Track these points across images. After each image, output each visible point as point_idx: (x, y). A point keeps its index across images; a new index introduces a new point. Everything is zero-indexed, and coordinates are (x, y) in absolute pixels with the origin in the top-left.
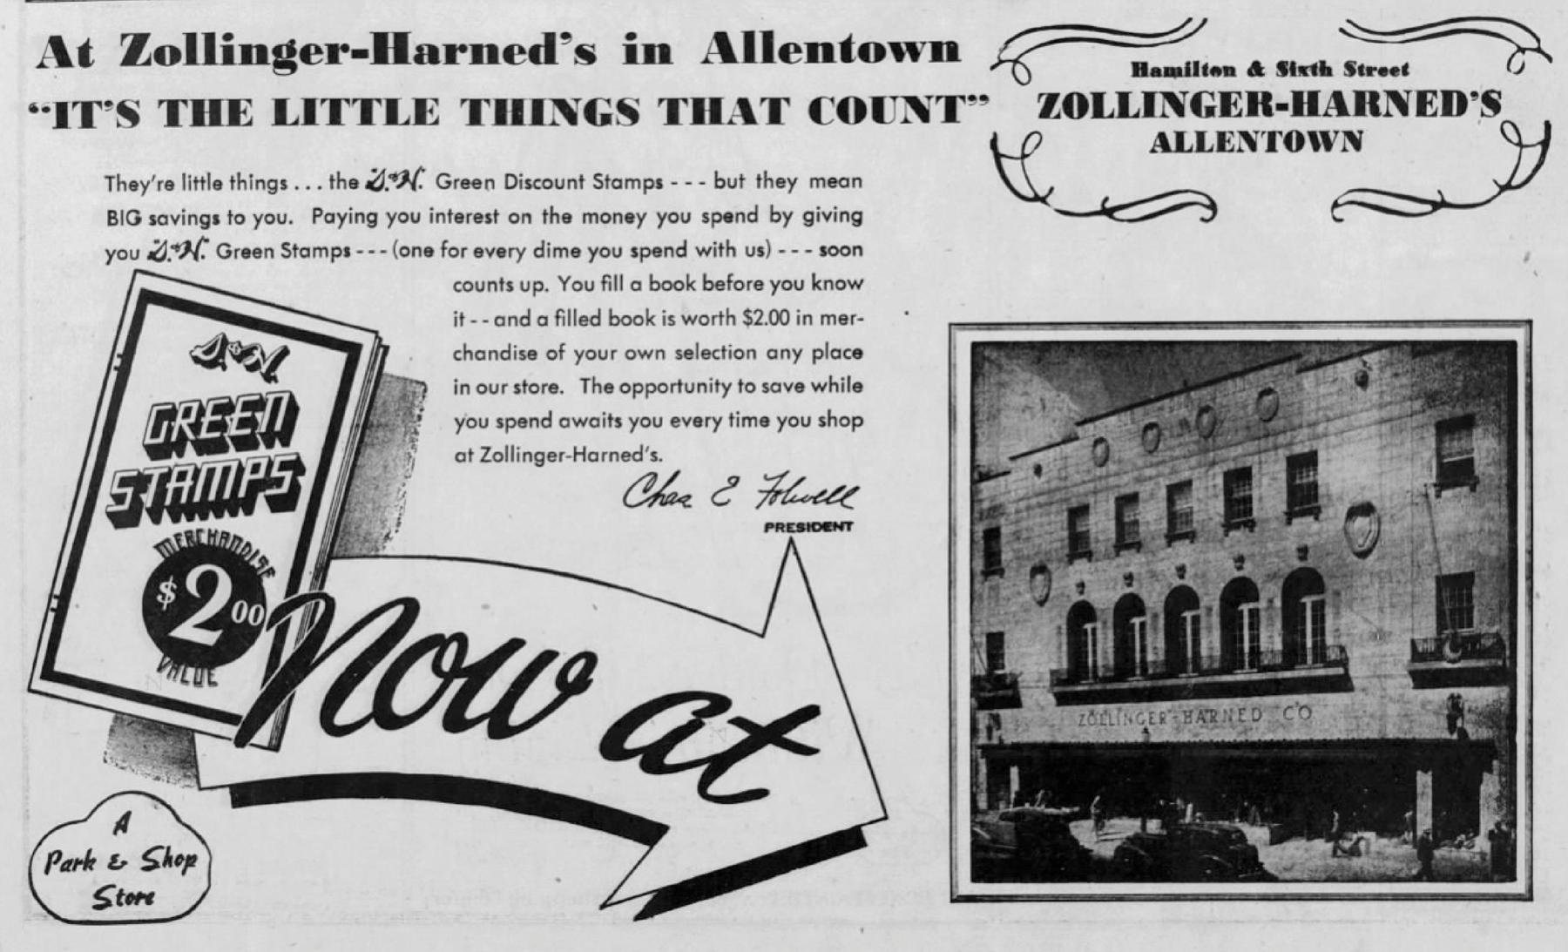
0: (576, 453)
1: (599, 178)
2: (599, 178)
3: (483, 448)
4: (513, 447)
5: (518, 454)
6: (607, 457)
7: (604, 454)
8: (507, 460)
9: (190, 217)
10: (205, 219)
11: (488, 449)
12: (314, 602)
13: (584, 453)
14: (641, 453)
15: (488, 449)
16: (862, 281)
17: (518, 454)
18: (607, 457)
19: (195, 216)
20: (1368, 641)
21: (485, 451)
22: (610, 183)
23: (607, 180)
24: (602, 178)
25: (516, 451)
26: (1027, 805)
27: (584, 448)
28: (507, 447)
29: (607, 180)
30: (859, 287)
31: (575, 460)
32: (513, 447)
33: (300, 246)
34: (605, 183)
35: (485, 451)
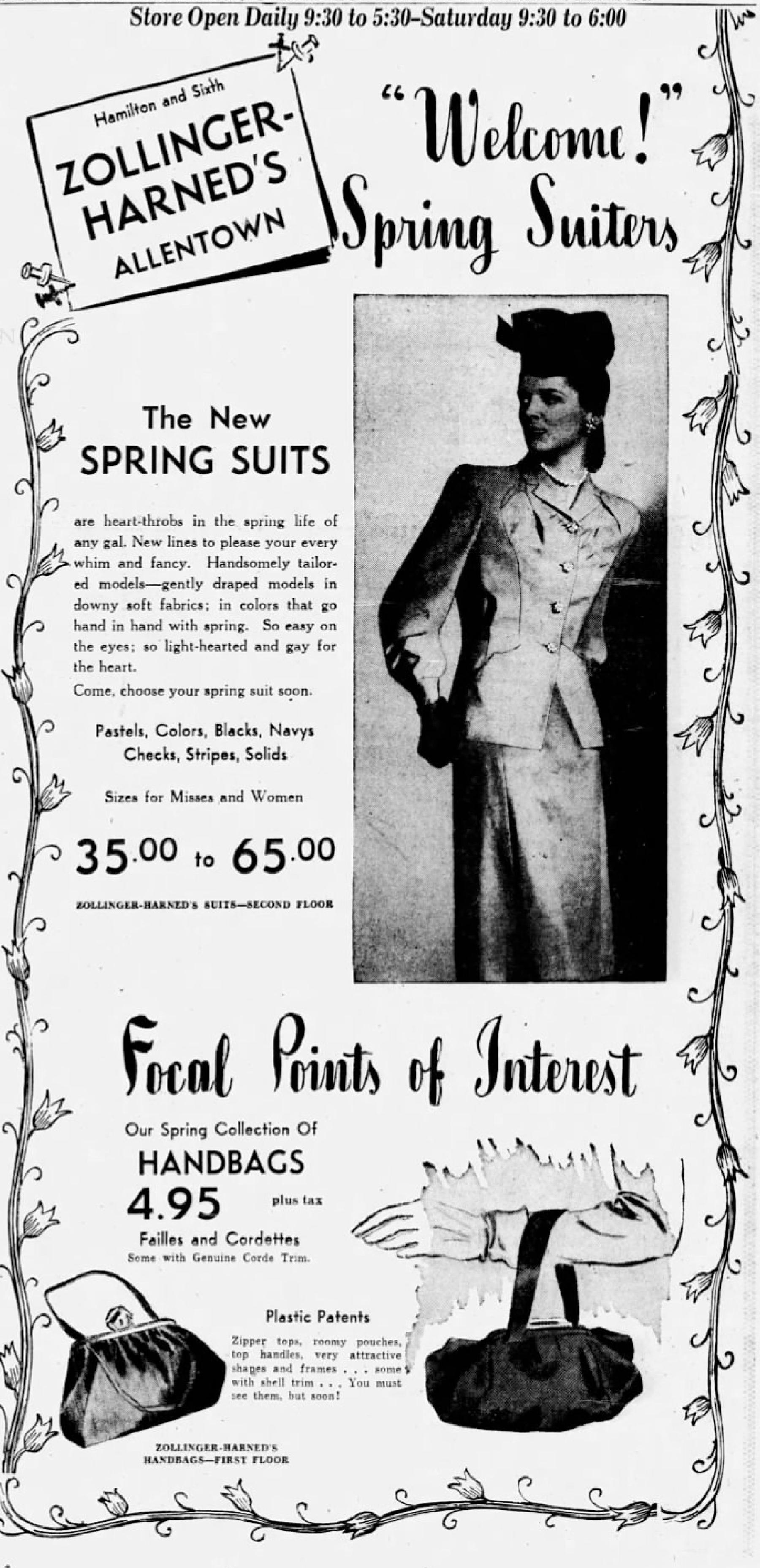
3: (59, 167)
16: (268, 416)
21: (65, 171)
22: (201, 861)
23: (198, 754)
27: (217, 557)
30: (264, 424)
35: (65, 171)
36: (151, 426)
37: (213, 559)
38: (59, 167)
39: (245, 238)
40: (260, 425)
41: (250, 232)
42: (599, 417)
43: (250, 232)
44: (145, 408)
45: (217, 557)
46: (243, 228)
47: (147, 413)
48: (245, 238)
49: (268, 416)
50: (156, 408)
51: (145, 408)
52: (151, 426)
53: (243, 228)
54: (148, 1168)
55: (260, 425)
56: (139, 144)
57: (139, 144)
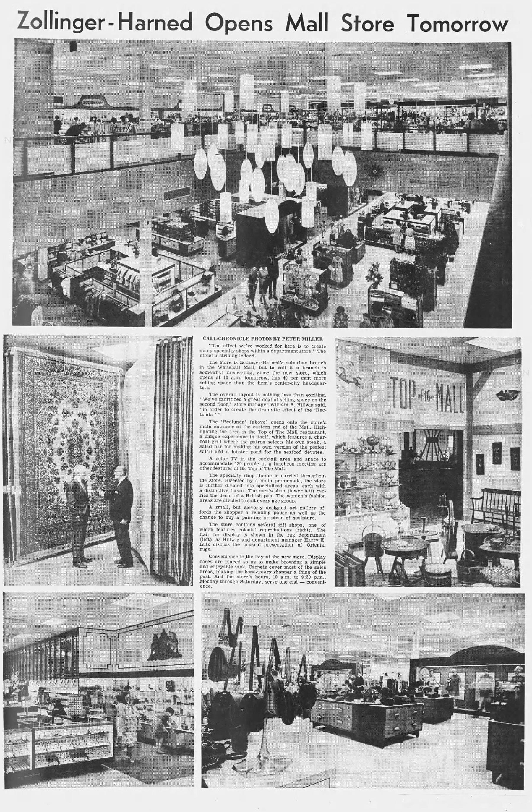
0: (121, 21)
1: (347, 18)
2: (347, 18)
3: (20, 12)
4: (51, 12)
5: (57, 20)
6: (153, 25)
7: (149, 22)
8: (46, 27)
9: (62, 20)
10: (78, 24)
11: (26, 13)
12: (190, 307)
13: (130, 21)
14: (190, 22)
15: (26, 13)
16: (506, 22)
17: (57, 20)
18: (153, 25)
19: (68, 20)
20: (501, 565)
21: (23, 15)
22: (360, 25)
23: (357, 21)
24: (352, 20)
25: (55, 16)
26: (495, 750)
27: (131, 14)
28: (46, 12)
29: (357, 21)
30: (503, 28)
31: (120, 28)
32: (51, 12)
33: (362, 19)
34: (354, 25)
36: (413, 30)
37: (126, 16)
38: (20, 12)
39: (497, 30)
40: (500, 28)
41: (500, 28)
42: (497, 124)
43: (500, 28)
44: (409, 15)
45: (131, 14)
46: (497, 24)
47: (410, 18)
48: (497, 30)
49: (506, 22)
50: (397, 379)
51: (409, 15)
52: (413, 30)
53: (497, 24)
54: (126, 25)
55: (500, 28)
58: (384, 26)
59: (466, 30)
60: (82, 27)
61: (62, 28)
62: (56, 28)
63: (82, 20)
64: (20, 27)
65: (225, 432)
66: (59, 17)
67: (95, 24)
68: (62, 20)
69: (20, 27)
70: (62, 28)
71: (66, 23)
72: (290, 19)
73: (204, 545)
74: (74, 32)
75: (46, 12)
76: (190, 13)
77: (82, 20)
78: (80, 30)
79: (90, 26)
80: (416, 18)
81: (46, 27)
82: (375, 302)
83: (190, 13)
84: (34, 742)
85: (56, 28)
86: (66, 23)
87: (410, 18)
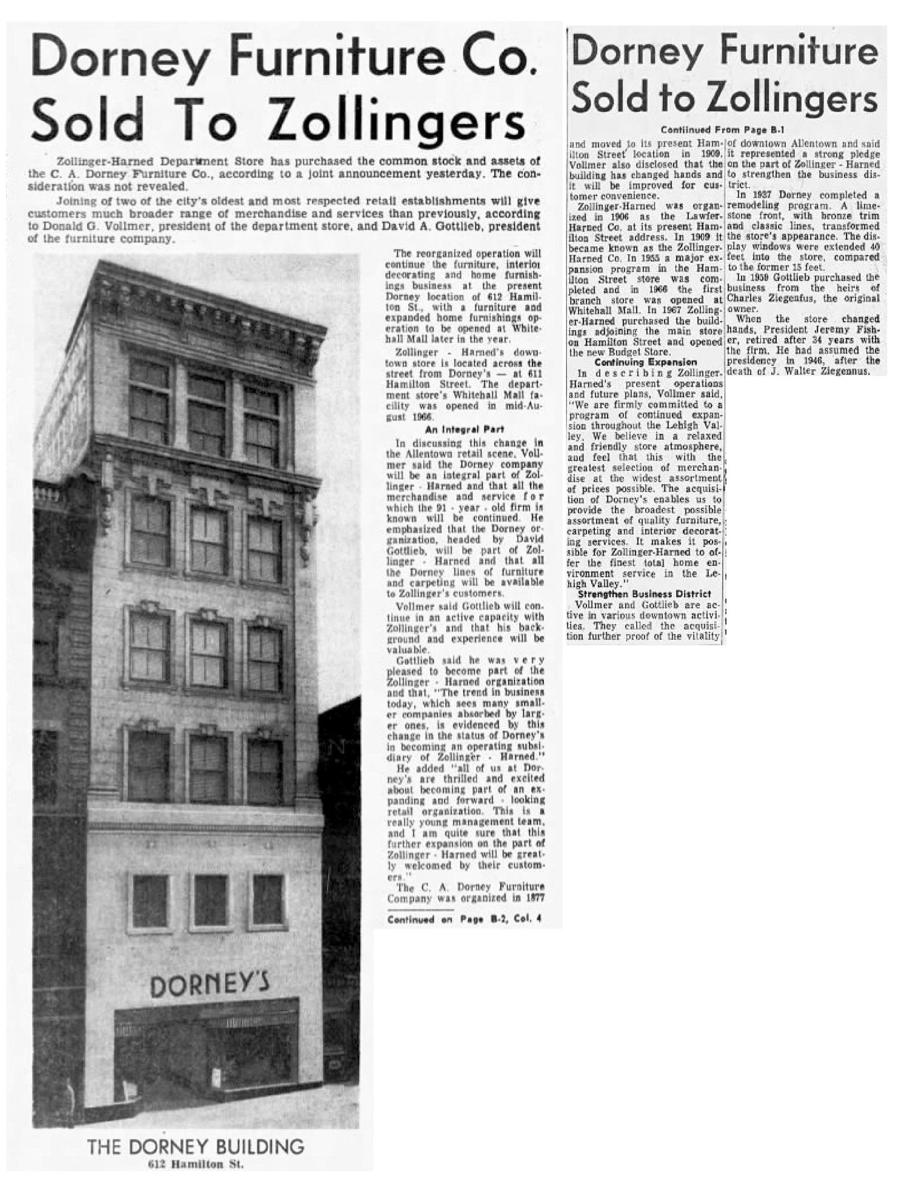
3: (274, 100)
4: (767, 81)
5: (777, 95)
9: (787, 96)
10: (815, 101)
11: (721, 84)
15: (721, 84)
17: (777, 95)
19: (797, 95)
21: (716, 87)
25: (773, 89)
28: (757, 82)
32: (767, 81)
38: (274, 100)
47: (182, 108)
56: (103, 99)
57: (103, 99)
58: (421, 61)
59: (106, 72)
60: (439, 134)
61: (389, 136)
62: (777, 109)
63: (821, 95)
64: (276, 135)
65: (621, 479)
66: (782, 90)
67: (474, 124)
68: (787, 96)
69: (276, 135)
70: (786, 109)
71: (792, 101)
72: (693, 60)
73: (398, 551)
74: (808, 116)
75: (342, 99)
76: (140, 99)
77: (821, 95)
78: (434, 141)
79: (464, 131)
80: (195, 108)
81: (757, 109)
82: (122, 1074)
83: (140, 99)
84: (206, 544)
85: (777, 109)
86: (792, 101)
87: (182, 108)
